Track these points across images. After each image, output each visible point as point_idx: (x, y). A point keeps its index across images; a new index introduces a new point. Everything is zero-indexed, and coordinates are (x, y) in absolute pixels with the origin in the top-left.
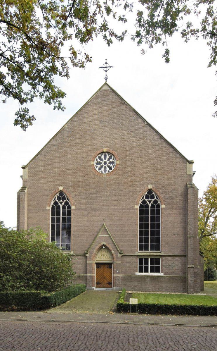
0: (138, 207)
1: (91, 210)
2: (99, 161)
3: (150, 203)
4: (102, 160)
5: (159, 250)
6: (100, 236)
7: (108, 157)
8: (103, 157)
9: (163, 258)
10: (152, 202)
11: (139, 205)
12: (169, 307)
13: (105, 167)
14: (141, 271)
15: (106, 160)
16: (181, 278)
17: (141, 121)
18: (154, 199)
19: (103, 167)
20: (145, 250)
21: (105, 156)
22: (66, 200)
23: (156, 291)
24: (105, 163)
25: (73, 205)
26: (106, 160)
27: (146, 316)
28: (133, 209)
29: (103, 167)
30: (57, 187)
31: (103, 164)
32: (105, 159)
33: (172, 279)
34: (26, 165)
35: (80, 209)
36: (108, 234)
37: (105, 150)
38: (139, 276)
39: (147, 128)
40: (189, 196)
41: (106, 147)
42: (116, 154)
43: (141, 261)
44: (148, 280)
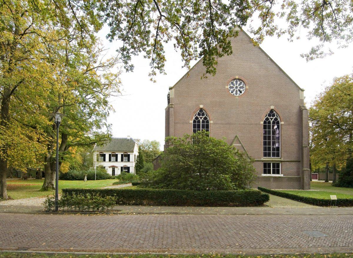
0: (192, 122)
1: (226, 124)
2: (232, 85)
3: (201, 119)
4: (234, 85)
5: (279, 156)
6: (234, 145)
7: (239, 83)
8: (235, 82)
9: (283, 163)
10: (203, 119)
11: (193, 120)
12: (145, 202)
13: (234, 90)
14: (265, 173)
15: (238, 85)
16: (296, 178)
17: (265, 56)
18: (204, 116)
19: (235, 91)
20: (268, 157)
21: (236, 82)
22: (205, 116)
23: (294, 189)
24: (237, 87)
25: (212, 120)
26: (238, 85)
27: (239, 208)
28: (259, 124)
29: (235, 91)
30: (198, 105)
31: (235, 88)
32: (236, 85)
33: (290, 179)
34: (172, 86)
35: (216, 124)
36: (240, 143)
37: (237, 77)
38: (265, 177)
39: (269, 62)
40: (303, 116)
41: (238, 75)
42: (246, 81)
43: (265, 165)
44: (272, 180)
